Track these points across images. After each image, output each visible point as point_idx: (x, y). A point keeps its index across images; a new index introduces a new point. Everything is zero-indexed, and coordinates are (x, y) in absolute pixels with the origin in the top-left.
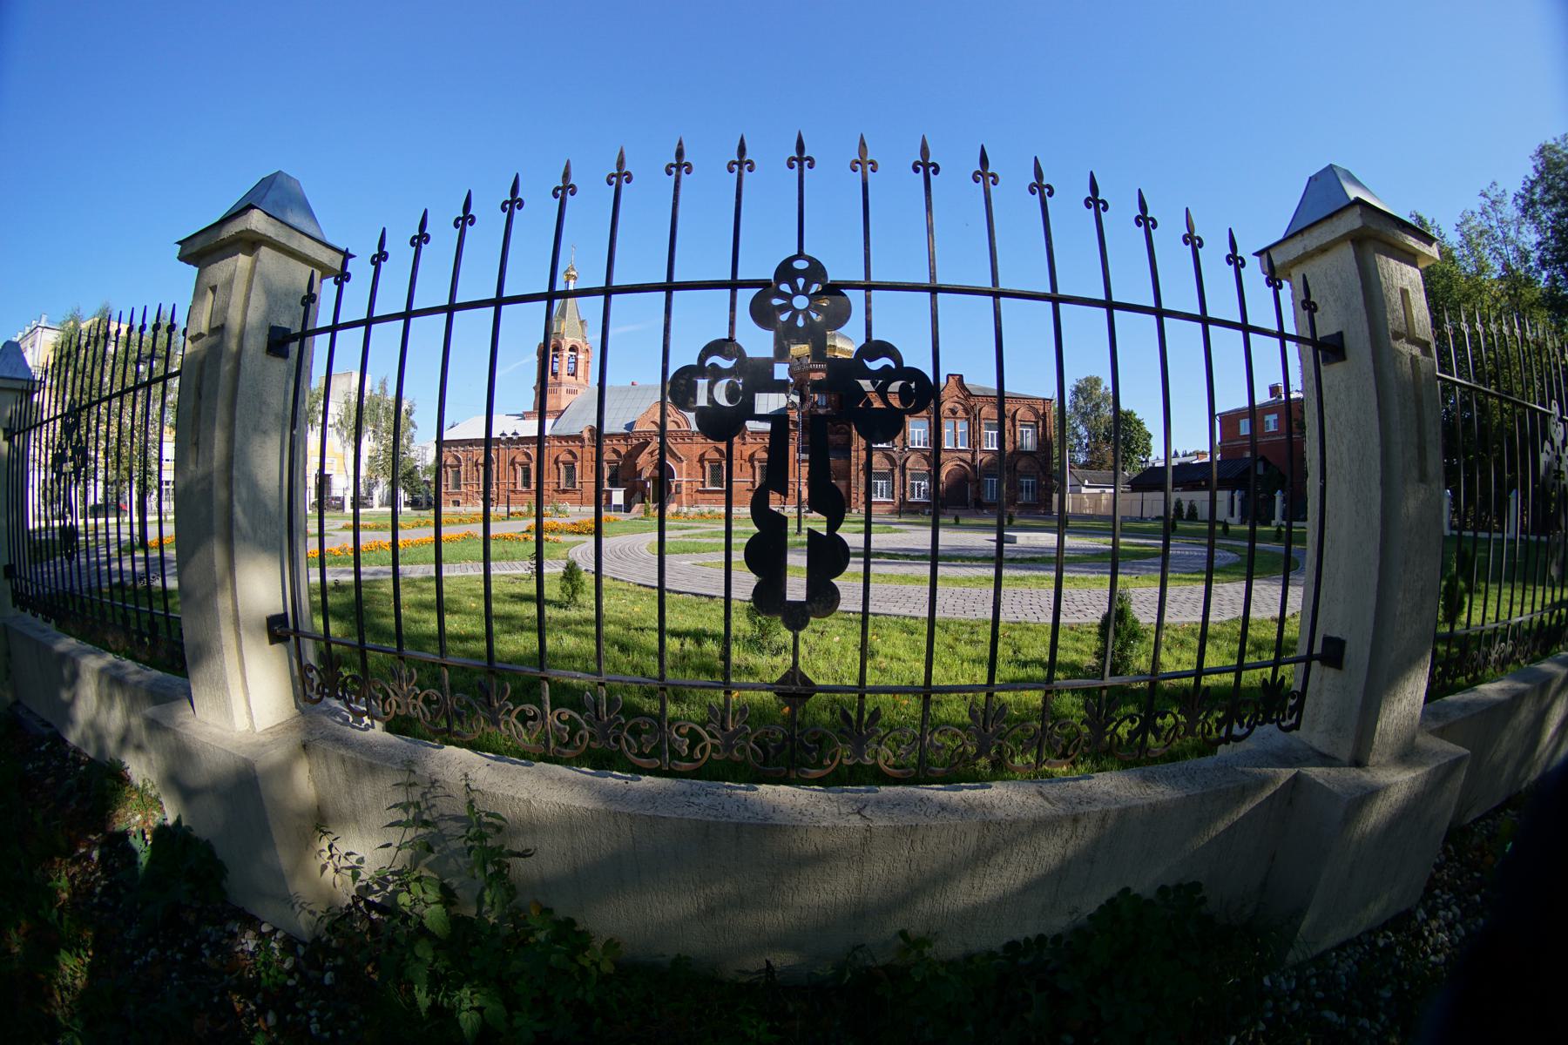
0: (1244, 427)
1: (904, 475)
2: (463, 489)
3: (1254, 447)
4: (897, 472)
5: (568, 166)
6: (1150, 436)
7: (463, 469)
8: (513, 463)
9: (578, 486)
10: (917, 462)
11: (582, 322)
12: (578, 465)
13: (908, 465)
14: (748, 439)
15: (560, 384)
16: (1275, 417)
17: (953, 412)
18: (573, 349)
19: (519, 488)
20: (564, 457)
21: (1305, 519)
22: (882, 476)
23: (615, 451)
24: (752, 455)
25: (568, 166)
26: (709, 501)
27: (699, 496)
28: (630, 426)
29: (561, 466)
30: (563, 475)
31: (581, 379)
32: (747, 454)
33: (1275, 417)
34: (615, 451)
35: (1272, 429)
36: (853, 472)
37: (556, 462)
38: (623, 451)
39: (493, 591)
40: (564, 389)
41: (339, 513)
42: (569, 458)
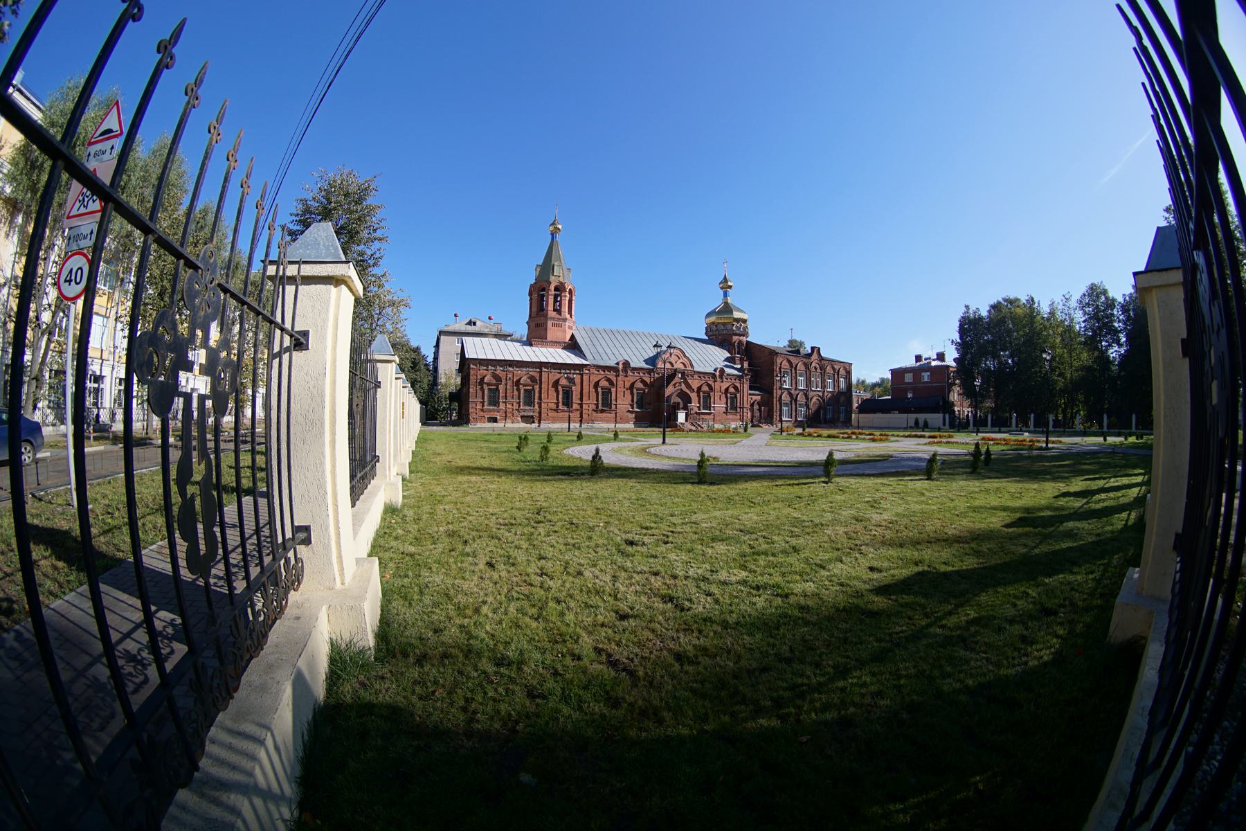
0: (909, 378)
2: (502, 406)
3: (367, 361)
5: (184, 21)
14: (630, 373)
15: (565, 320)
19: (561, 407)
20: (604, 383)
21: (1146, 424)
22: (786, 405)
23: (643, 381)
24: (633, 384)
25: (184, 21)
32: (723, 389)
34: (643, 381)
35: (926, 379)
38: (648, 380)
39: (226, 520)
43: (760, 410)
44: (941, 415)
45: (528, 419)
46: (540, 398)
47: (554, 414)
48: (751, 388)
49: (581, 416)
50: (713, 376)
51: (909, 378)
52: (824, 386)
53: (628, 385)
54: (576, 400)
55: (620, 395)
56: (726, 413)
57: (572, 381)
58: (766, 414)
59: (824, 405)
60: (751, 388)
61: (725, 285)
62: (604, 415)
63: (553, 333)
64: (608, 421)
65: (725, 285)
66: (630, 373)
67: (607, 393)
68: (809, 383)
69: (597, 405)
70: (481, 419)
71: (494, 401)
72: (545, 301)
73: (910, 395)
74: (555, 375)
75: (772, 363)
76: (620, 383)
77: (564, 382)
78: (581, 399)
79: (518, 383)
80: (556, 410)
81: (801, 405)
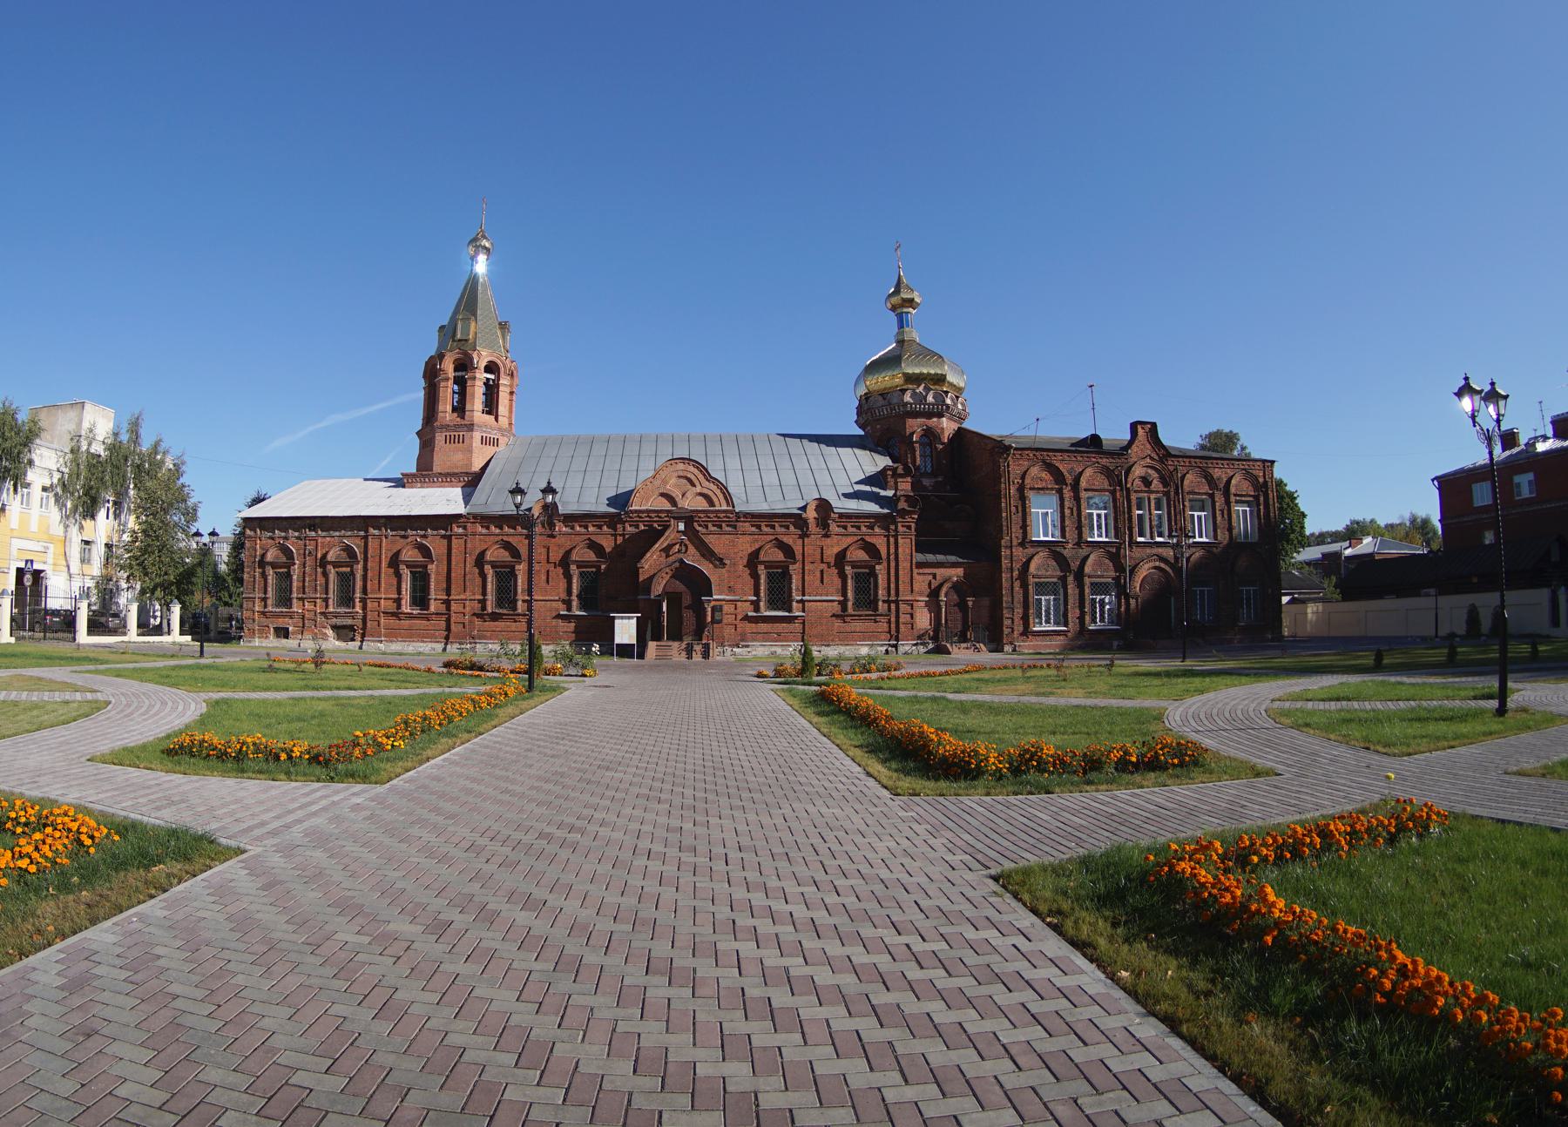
1: (1081, 586)
2: (296, 607)
4: (1070, 579)
6: (1304, 515)
7: (296, 571)
8: (394, 562)
9: (521, 607)
10: (1099, 564)
11: (503, 326)
12: (521, 569)
13: (1087, 569)
14: (834, 528)
15: (470, 427)
16: (1531, 476)
17: (1146, 481)
18: (491, 368)
19: (406, 608)
22: (1042, 588)
23: (594, 546)
24: (841, 558)
26: (766, 637)
27: (749, 627)
28: (621, 500)
29: (489, 570)
30: (407, 586)
31: (503, 421)
33: (1531, 476)
34: (594, 546)
35: (1526, 493)
36: (1005, 584)
37: (480, 561)
38: (608, 544)
40: (477, 435)
41: (63, 648)
42: (505, 556)
43: (962, 606)
44: (1543, 595)
45: (344, 632)
46: (365, 591)
47: (393, 622)
48: (921, 547)
49: (448, 629)
50: (798, 520)
51: (1482, 495)
52: (1179, 529)
53: (556, 556)
54: (435, 594)
55: (812, 579)
56: (842, 616)
57: (425, 551)
58: (979, 614)
59: (1167, 588)
60: (921, 547)
61: (901, 306)
62: (500, 624)
63: (445, 457)
64: (423, 636)
65: (901, 306)
66: (560, 527)
67: (506, 577)
68: (1122, 521)
69: (843, 604)
70: (263, 632)
71: (285, 599)
72: (453, 381)
73: (1489, 538)
74: (385, 544)
75: (996, 477)
76: (539, 553)
77: (410, 554)
78: (448, 591)
79: (323, 562)
80: (396, 615)
81: (1099, 588)
